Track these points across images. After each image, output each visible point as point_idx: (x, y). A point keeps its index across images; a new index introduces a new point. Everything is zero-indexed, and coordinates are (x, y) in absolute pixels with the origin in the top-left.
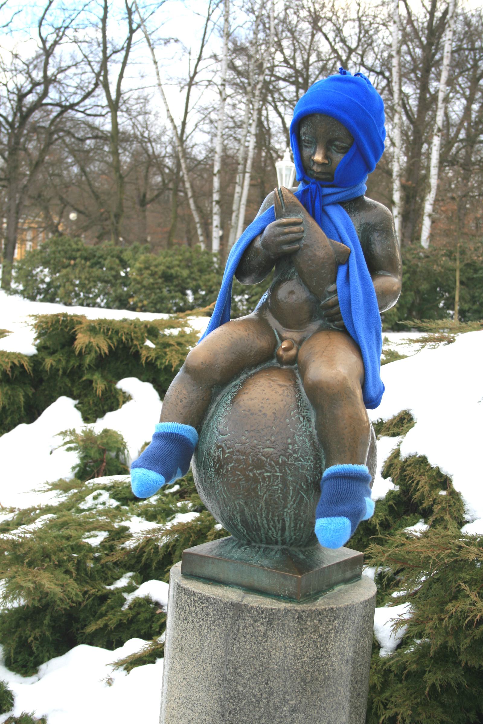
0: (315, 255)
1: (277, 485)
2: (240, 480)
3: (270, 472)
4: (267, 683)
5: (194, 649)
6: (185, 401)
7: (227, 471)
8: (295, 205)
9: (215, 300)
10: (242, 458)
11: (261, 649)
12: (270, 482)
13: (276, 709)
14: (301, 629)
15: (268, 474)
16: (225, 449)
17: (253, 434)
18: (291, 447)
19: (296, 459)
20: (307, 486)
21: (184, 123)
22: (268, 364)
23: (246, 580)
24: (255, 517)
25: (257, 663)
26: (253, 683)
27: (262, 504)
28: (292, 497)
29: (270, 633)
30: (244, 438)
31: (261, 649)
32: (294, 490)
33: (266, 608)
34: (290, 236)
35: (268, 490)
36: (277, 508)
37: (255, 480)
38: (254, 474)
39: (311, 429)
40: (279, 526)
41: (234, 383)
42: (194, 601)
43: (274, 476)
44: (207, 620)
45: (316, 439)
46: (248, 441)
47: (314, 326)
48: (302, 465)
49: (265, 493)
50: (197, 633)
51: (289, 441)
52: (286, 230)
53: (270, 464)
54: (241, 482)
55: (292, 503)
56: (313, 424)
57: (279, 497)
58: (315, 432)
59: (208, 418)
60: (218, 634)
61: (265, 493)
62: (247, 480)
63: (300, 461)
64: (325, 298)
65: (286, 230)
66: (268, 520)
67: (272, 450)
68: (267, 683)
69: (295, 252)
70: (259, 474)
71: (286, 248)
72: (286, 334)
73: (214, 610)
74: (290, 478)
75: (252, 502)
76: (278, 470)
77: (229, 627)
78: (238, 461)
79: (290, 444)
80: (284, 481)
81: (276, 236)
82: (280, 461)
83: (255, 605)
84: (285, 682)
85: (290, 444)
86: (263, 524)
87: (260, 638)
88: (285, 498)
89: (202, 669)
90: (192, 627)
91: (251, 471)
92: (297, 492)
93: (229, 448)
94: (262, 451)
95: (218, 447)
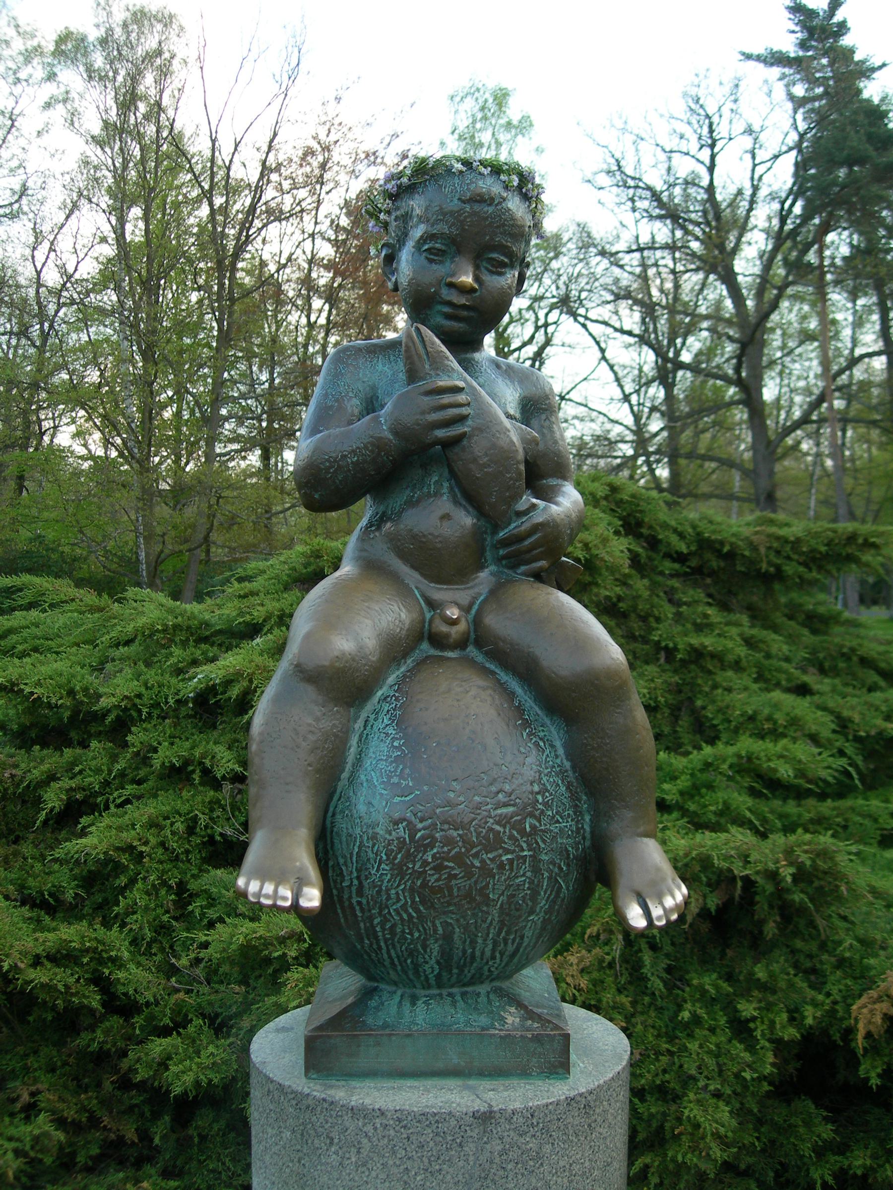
1: (524, 875)
2: (455, 876)
3: (513, 852)
7: (425, 863)
9: (349, 533)
10: (455, 834)
11: (534, 1181)
12: (511, 869)
14: (590, 1126)
15: (509, 856)
16: (415, 821)
20: (568, 865)
21: (231, 161)
22: (417, 655)
23: (455, 1059)
24: (473, 943)
28: (545, 893)
30: (452, 795)
31: (534, 1181)
32: (550, 878)
33: (538, 1107)
36: (520, 916)
38: (483, 861)
39: (558, 761)
40: (511, 948)
41: (379, 693)
43: (519, 857)
46: (462, 799)
47: (485, 578)
48: (561, 830)
49: (502, 894)
51: (536, 788)
52: (447, 399)
53: (511, 837)
54: (453, 882)
55: (544, 902)
56: (561, 751)
58: (567, 764)
59: (348, 767)
60: (449, 1177)
61: (502, 894)
62: (469, 875)
63: (557, 822)
64: (509, 524)
65: (447, 399)
66: (495, 943)
67: (511, 809)
69: (457, 440)
71: (441, 433)
72: (439, 593)
74: (544, 857)
76: (525, 846)
77: (471, 1158)
78: (449, 842)
79: (538, 793)
81: (423, 413)
82: (528, 829)
83: (518, 1105)
85: (538, 793)
86: (483, 953)
87: (531, 1163)
90: (383, 1176)
91: (476, 855)
92: (553, 880)
93: (421, 821)
94: (493, 813)
95: (396, 823)
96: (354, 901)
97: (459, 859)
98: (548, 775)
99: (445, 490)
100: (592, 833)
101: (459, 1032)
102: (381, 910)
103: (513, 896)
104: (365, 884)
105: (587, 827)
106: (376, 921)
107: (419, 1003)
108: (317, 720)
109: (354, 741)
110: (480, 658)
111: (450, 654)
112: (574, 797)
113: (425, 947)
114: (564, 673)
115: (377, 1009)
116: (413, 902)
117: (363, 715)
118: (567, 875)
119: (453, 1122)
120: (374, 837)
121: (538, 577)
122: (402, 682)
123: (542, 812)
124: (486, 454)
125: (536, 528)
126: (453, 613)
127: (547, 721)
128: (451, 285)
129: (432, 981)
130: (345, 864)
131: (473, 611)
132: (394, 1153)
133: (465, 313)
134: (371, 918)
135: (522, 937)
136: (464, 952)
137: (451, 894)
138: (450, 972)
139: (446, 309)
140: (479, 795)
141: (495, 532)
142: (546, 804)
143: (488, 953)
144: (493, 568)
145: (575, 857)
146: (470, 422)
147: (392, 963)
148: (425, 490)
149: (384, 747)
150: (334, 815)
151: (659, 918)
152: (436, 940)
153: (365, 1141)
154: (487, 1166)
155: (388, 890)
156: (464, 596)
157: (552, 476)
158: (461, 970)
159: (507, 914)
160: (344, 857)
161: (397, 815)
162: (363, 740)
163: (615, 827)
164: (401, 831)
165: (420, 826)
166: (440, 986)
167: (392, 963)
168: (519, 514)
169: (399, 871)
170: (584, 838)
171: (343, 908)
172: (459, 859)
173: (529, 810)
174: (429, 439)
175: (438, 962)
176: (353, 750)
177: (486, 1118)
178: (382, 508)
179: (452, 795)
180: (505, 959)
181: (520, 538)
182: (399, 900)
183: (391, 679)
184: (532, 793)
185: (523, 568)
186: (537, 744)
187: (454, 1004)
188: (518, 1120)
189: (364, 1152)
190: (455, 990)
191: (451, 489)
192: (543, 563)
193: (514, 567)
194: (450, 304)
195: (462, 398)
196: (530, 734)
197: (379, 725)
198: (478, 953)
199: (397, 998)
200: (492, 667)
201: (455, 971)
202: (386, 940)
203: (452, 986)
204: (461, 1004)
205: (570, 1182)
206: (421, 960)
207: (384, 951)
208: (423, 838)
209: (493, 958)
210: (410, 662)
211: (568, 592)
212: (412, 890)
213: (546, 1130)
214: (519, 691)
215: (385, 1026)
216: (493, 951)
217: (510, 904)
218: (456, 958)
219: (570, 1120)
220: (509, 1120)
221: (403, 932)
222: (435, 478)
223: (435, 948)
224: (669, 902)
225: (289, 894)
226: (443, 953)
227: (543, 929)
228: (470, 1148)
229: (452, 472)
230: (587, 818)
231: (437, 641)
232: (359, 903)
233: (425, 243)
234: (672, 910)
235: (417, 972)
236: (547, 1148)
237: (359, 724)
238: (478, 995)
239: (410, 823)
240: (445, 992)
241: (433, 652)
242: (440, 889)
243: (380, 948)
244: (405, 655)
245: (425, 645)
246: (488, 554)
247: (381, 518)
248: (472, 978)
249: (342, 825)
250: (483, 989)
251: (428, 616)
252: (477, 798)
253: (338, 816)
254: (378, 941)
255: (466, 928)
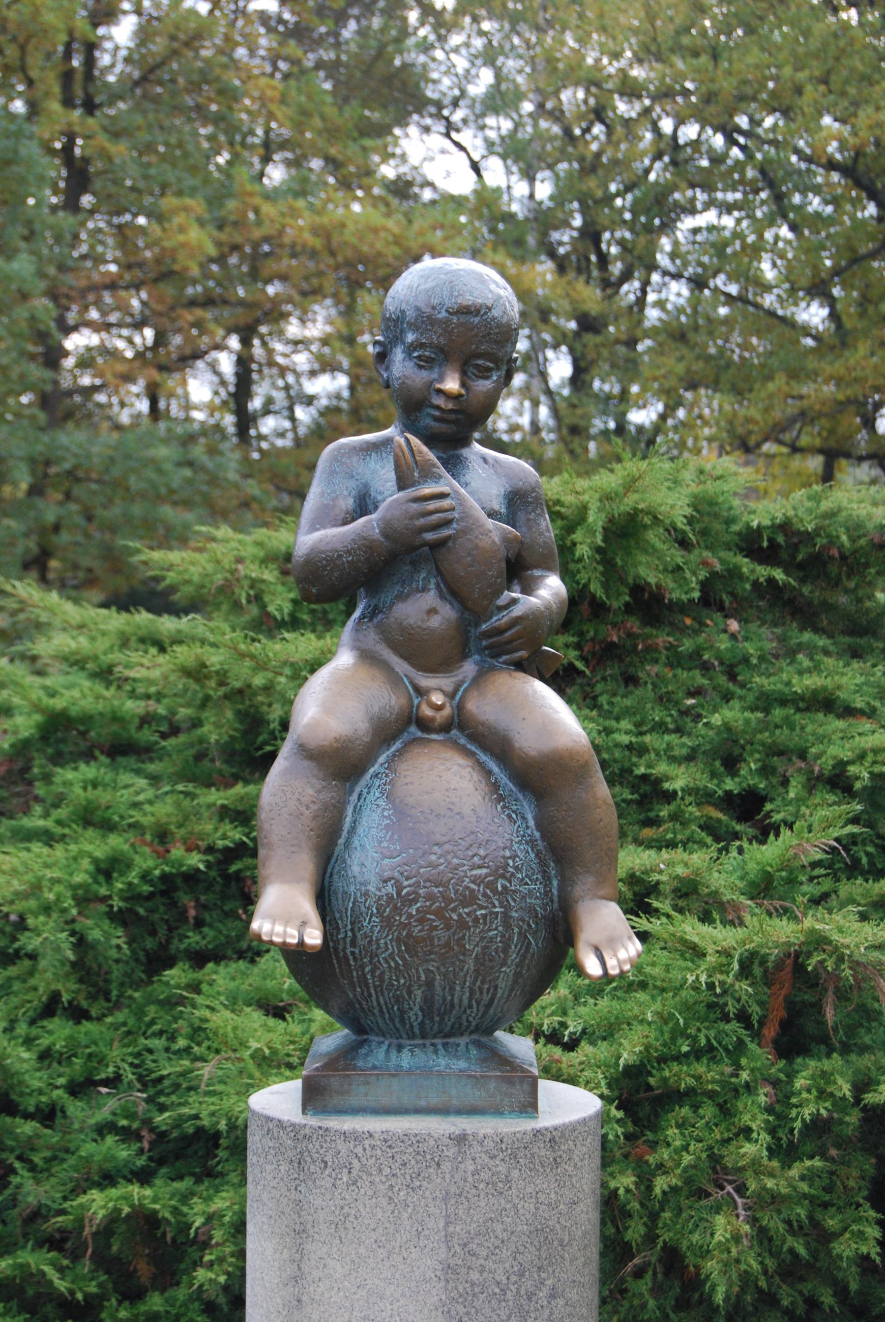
0: (477, 547)
2: (436, 927)
3: (486, 908)
4: (515, 1259)
5: (380, 1230)
6: (314, 807)
7: (410, 916)
8: (434, 465)
13: (529, 1299)
17: (447, 847)
18: (511, 862)
19: (522, 882)
20: (537, 924)
22: (405, 737)
23: (434, 1099)
24: (452, 989)
25: (499, 1227)
26: (495, 1262)
27: (470, 964)
29: (515, 1174)
30: (433, 857)
32: (520, 934)
34: (435, 517)
35: (482, 939)
37: (462, 924)
38: (460, 915)
40: (486, 998)
41: (372, 771)
42: (373, 1147)
43: (492, 913)
44: (404, 1175)
45: (541, 845)
47: (469, 668)
50: (384, 1202)
52: (432, 505)
53: (485, 895)
56: (532, 823)
57: (496, 950)
58: (537, 834)
59: (344, 834)
60: (428, 1193)
62: (448, 927)
65: (432, 505)
66: (472, 992)
68: (515, 1259)
69: (442, 543)
70: (468, 914)
71: (429, 536)
72: (426, 681)
73: (418, 1153)
74: (514, 914)
75: (453, 964)
77: (448, 1176)
78: (430, 897)
80: (506, 916)
83: (489, 1131)
84: (539, 1250)
86: (461, 1000)
88: (506, 950)
89: (400, 1259)
90: (370, 1193)
91: (454, 910)
92: (522, 935)
93: (407, 879)
95: (385, 881)
96: (348, 951)
97: (439, 913)
98: (520, 842)
99: (432, 586)
100: (559, 896)
101: (440, 1074)
102: (371, 958)
103: (486, 947)
104: (359, 935)
105: (555, 892)
106: (367, 969)
107: (405, 1050)
108: (319, 792)
109: (350, 810)
110: (463, 741)
111: (434, 737)
112: (543, 863)
113: (409, 993)
114: (533, 753)
115: (367, 1055)
116: (400, 950)
117: (357, 790)
118: (535, 932)
119: (432, 1143)
120: (366, 894)
121: (520, 666)
122: (391, 760)
123: (513, 875)
124: (469, 554)
125: (518, 620)
126: (437, 698)
127: (520, 796)
128: (440, 392)
129: (417, 1030)
130: (341, 918)
131: (458, 698)
132: (380, 1171)
133: (453, 417)
134: (362, 967)
135: (496, 988)
136: (444, 999)
137: (432, 945)
138: (432, 1019)
139: (437, 413)
140: (456, 857)
141: (477, 625)
142: (517, 868)
143: (466, 1002)
144: (477, 657)
145: (543, 917)
146: (455, 525)
147: (381, 1011)
148: (414, 585)
149: (375, 816)
150: (331, 875)
151: (613, 968)
152: (420, 987)
153: (355, 1162)
154: (461, 1183)
155: (378, 940)
156: (446, 682)
157: (537, 567)
158: (442, 1016)
159: (483, 964)
160: (340, 912)
161: (387, 874)
162: (357, 811)
163: (578, 890)
164: (390, 889)
165: (406, 883)
166: (424, 1036)
167: (381, 1011)
168: (501, 609)
169: (387, 923)
170: (552, 901)
171: (338, 958)
172: (439, 913)
173: (500, 871)
174: (417, 542)
175: (421, 1009)
176: (348, 820)
177: (461, 1139)
178: (374, 602)
179: (433, 857)
180: (482, 1009)
181: (499, 631)
182: (387, 949)
183: (382, 759)
184: (504, 857)
185: (504, 658)
186: (509, 816)
187: (436, 1052)
188: (489, 1144)
189: (355, 1172)
190: (437, 1041)
191: (438, 586)
192: (523, 654)
193: (496, 656)
194: (438, 408)
195: (446, 503)
196: (504, 807)
197: (371, 797)
198: (456, 1001)
199: (385, 1047)
200: (473, 748)
201: (437, 1019)
202: (375, 987)
203: (435, 1037)
204: (442, 1051)
205: (537, 1209)
206: (406, 1006)
207: (374, 998)
208: (408, 894)
209: (470, 1006)
210: (398, 745)
211: (542, 679)
212: (398, 940)
213: (514, 1156)
214: (496, 769)
215: (375, 1068)
216: (470, 999)
217: (484, 954)
218: (437, 1005)
219: (536, 1150)
220: (481, 1143)
221: (390, 978)
222: (423, 575)
223: (418, 994)
224: (622, 954)
225: (296, 933)
226: (425, 1000)
227: (515, 982)
228: (446, 1166)
229: (438, 568)
230: (555, 883)
231: (424, 725)
232: (353, 953)
233: (415, 350)
234: (625, 962)
235: (402, 1020)
236: (515, 1174)
237: (355, 796)
238: (458, 1045)
239: (397, 881)
240: (428, 1042)
241: (419, 734)
242: (423, 939)
243: (370, 995)
244: (394, 737)
245: (413, 729)
246: (472, 646)
247: (374, 611)
248: (452, 1027)
249: (339, 884)
250: (463, 1041)
251: (416, 702)
252: (455, 861)
253: (335, 877)
254: (368, 988)
255: (445, 975)
